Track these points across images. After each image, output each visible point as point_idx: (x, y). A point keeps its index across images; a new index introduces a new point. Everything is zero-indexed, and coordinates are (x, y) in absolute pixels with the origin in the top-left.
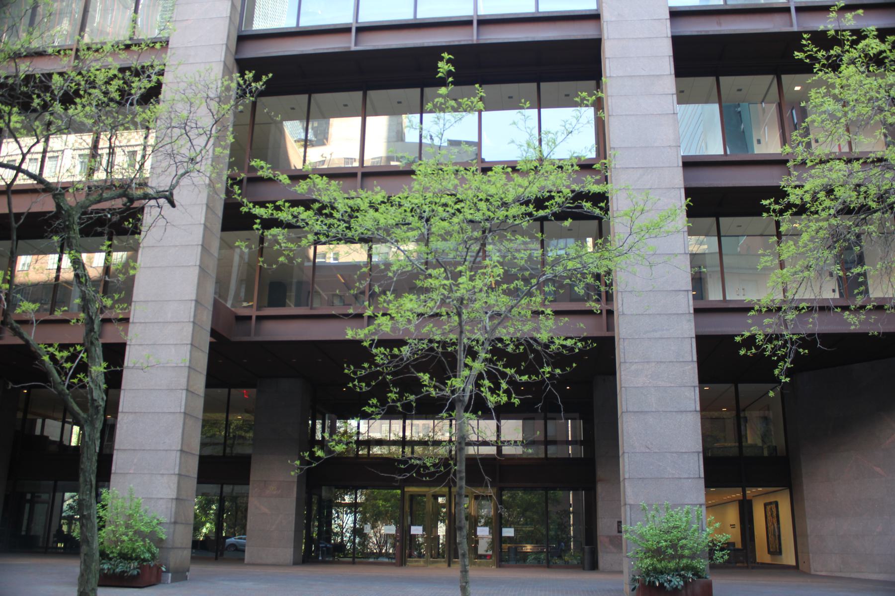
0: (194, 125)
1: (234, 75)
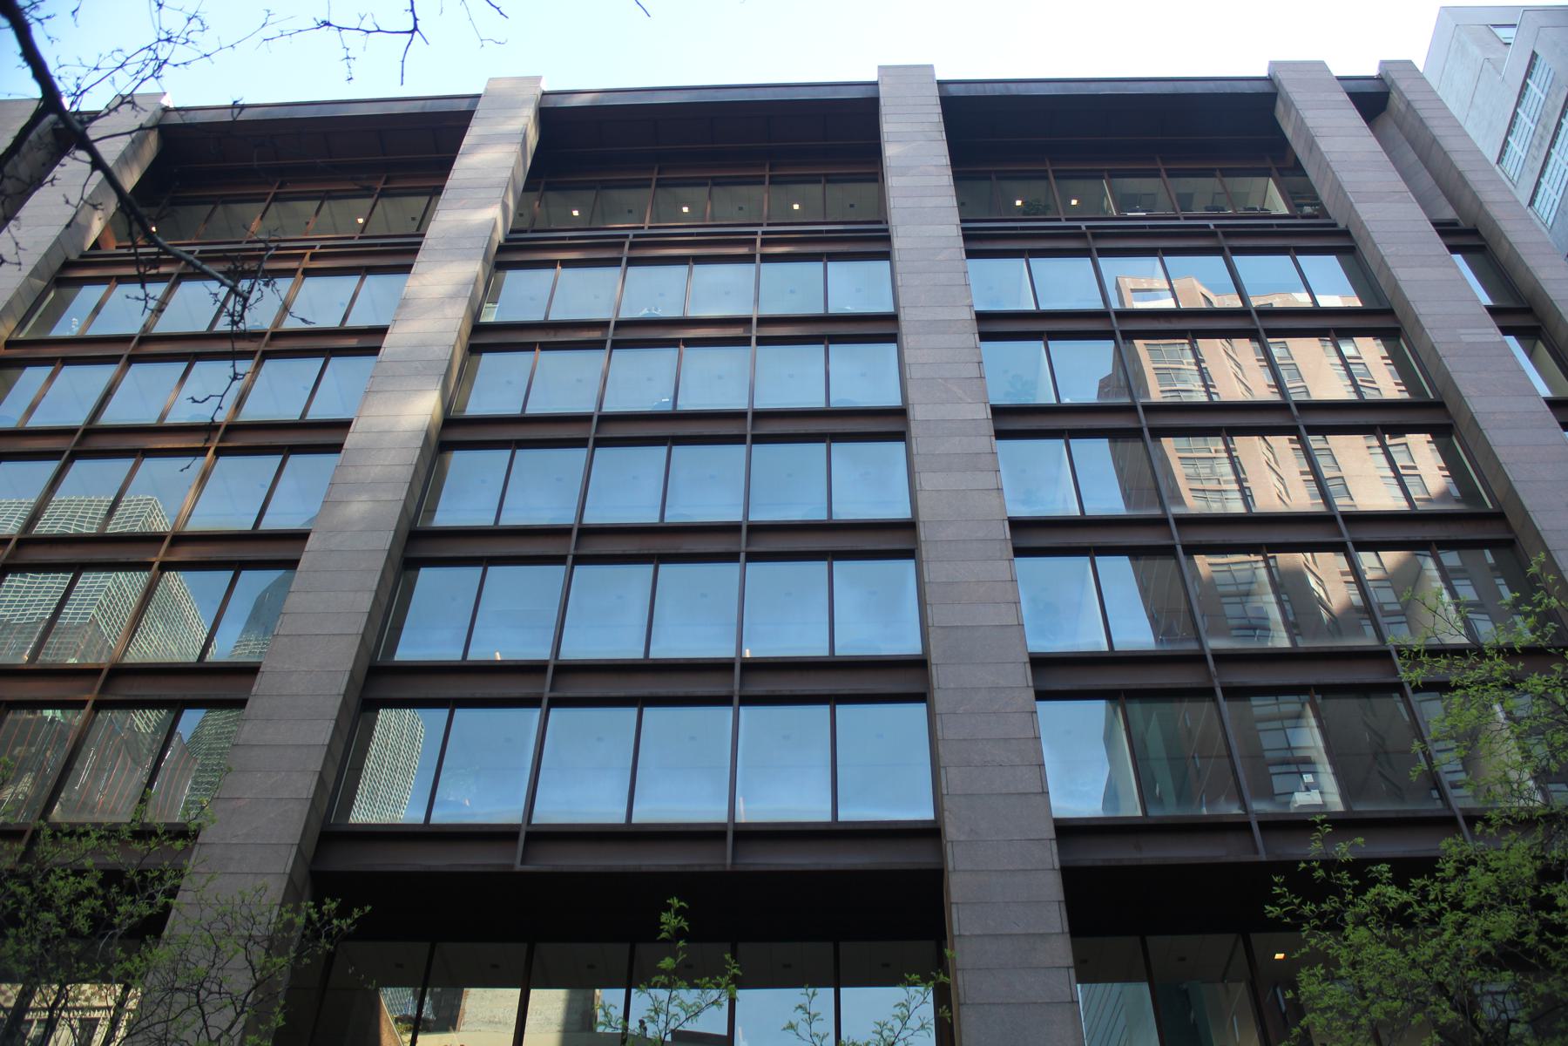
0: (215, 988)
1: (303, 904)
